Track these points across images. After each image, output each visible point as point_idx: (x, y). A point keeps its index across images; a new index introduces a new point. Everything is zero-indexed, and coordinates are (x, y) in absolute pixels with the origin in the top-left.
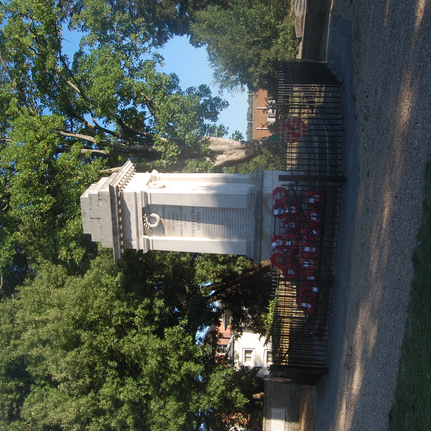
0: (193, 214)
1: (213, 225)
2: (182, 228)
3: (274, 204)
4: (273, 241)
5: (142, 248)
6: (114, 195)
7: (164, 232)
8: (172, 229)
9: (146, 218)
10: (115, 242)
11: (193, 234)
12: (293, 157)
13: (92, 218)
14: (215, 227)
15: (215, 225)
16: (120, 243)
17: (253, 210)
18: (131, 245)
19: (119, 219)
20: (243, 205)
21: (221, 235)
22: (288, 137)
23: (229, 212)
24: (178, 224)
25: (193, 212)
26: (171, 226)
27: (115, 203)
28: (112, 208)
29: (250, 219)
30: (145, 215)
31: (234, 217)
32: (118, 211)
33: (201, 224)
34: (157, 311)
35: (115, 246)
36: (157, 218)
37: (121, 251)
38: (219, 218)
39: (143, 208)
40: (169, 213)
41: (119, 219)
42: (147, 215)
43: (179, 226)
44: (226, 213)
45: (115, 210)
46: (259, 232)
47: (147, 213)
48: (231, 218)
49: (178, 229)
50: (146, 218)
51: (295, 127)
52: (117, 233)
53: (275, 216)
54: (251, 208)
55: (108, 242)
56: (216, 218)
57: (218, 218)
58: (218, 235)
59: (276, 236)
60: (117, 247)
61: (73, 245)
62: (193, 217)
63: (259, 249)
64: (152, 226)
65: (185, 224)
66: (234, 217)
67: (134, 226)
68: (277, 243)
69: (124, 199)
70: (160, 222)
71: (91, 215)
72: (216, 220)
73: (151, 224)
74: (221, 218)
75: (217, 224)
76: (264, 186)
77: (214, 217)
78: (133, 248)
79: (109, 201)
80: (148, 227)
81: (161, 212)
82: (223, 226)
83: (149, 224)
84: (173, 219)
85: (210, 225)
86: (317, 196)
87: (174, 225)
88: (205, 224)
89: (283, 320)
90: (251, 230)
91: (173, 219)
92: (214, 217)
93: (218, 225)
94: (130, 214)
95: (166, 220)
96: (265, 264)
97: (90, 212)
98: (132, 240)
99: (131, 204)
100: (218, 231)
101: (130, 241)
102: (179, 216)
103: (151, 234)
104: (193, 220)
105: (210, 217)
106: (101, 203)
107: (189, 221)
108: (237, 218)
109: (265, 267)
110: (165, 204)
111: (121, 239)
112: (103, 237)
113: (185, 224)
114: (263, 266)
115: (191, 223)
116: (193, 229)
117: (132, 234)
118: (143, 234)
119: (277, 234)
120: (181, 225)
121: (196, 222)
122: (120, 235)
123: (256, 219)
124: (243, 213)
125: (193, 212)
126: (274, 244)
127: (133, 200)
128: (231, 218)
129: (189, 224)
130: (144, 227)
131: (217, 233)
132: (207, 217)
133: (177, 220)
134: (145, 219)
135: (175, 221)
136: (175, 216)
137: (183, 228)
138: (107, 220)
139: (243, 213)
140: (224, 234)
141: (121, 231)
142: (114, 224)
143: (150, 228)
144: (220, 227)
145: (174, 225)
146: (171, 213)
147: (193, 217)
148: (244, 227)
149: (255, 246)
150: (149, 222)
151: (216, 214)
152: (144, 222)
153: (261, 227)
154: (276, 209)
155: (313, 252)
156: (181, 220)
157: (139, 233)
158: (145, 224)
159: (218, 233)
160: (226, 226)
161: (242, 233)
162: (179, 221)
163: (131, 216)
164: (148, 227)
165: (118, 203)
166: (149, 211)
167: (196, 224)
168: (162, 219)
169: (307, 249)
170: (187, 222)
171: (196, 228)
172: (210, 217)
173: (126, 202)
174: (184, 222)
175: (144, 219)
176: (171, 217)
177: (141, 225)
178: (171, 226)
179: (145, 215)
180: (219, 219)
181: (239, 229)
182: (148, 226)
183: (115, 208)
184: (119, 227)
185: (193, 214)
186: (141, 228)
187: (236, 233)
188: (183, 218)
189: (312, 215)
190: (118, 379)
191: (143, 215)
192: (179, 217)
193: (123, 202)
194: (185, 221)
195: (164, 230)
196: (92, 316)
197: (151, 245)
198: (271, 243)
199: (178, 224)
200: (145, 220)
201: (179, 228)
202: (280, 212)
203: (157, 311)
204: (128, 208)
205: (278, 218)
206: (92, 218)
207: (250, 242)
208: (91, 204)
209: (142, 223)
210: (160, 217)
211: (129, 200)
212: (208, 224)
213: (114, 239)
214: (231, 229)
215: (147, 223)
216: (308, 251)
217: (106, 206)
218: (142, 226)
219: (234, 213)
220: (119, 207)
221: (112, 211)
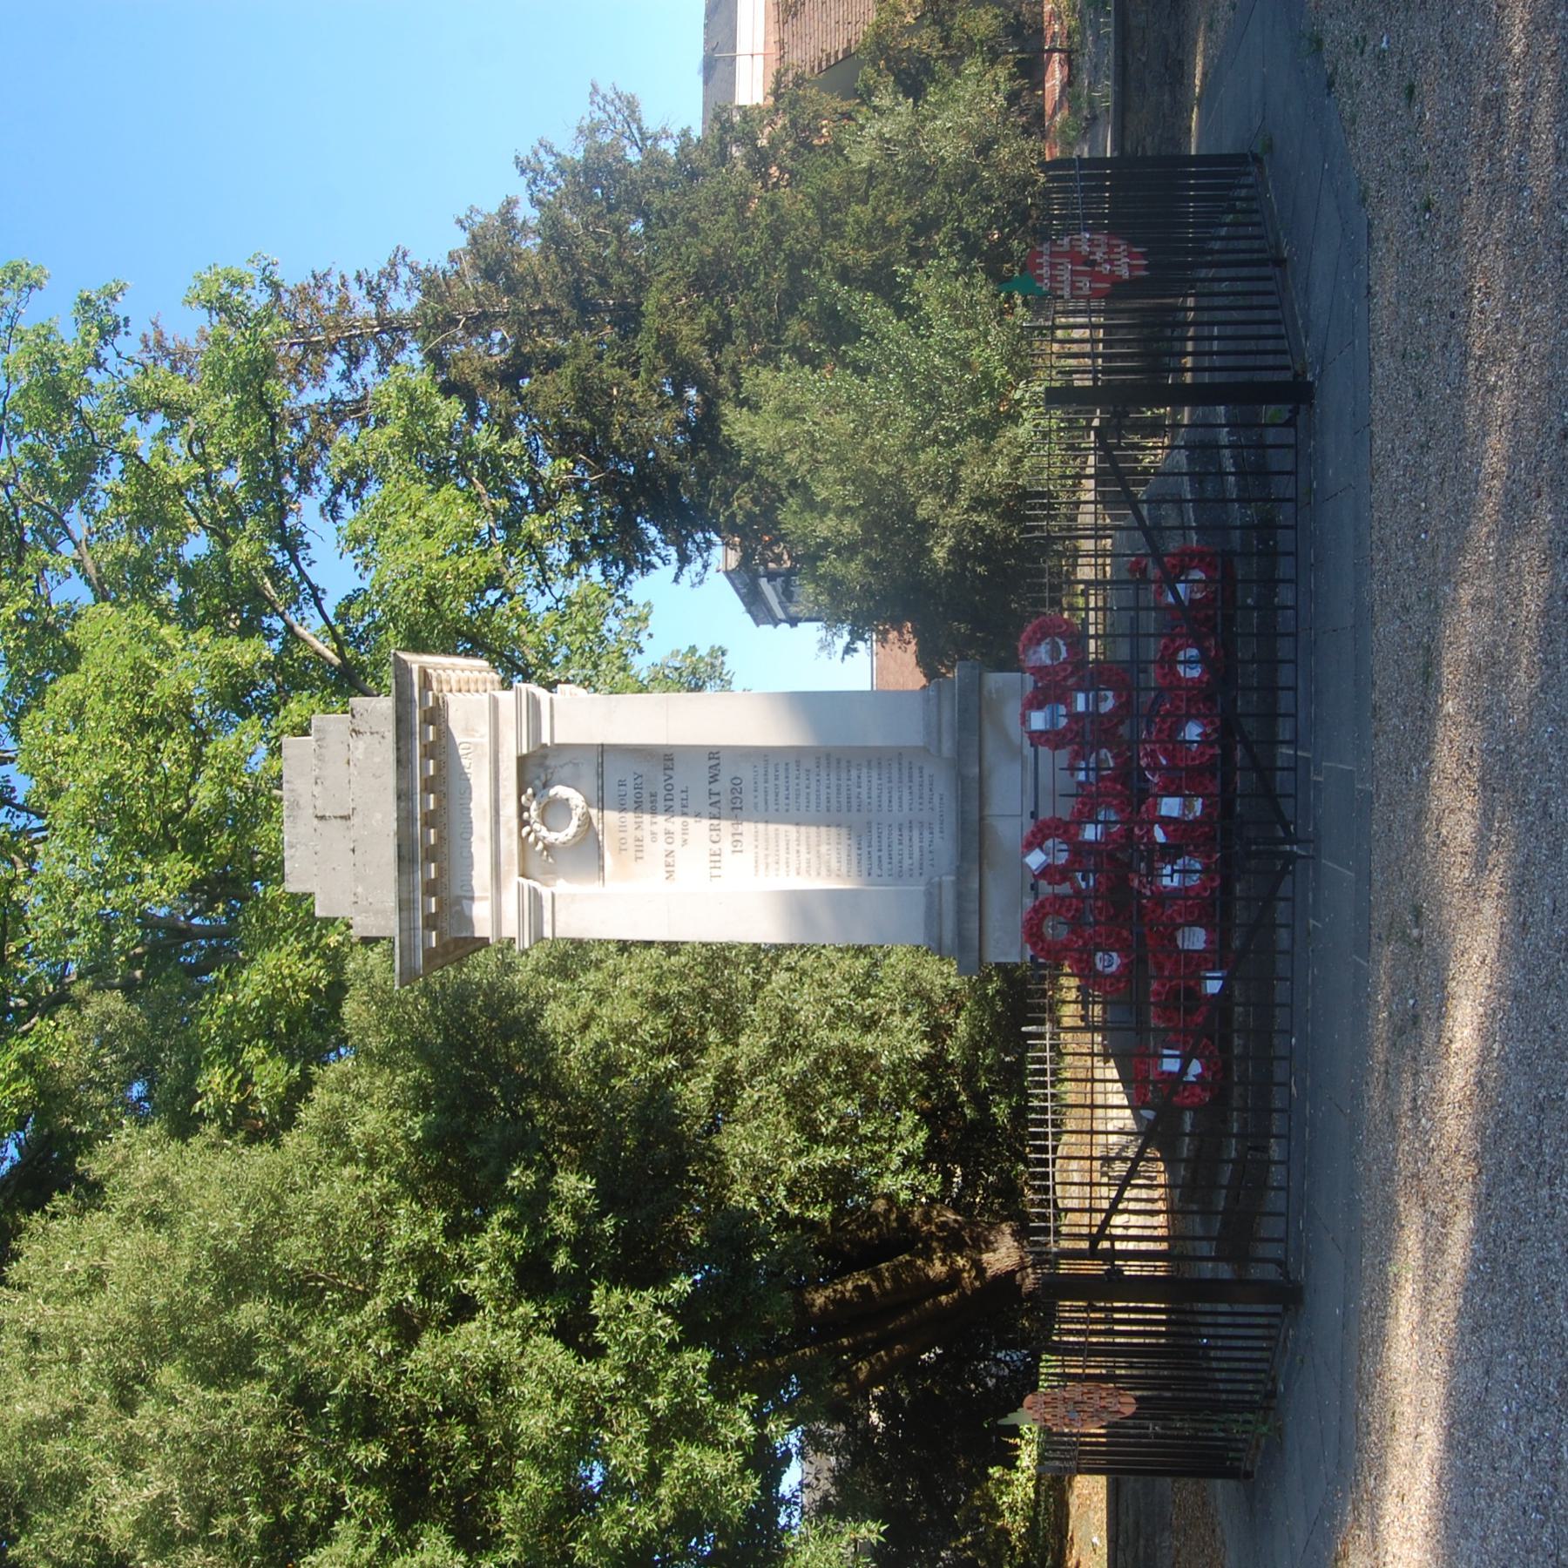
0: (715, 787)
1: (792, 829)
2: (670, 848)
3: (1029, 688)
4: (1029, 846)
5: (510, 929)
6: (412, 700)
7: (602, 868)
8: (631, 852)
9: (534, 806)
10: (405, 896)
11: (716, 872)
12: (1093, 561)
13: (322, 818)
14: (803, 838)
15: (803, 829)
16: (426, 906)
17: (947, 747)
18: (469, 922)
19: (424, 802)
20: (911, 734)
21: (824, 871)
22: (1073, 282)
23: (854, 773)
24: (655, 828)
25: (714, 779)
26: (631, 841)
27: (412, 734)
28: (398, 742)
29: (936, 799)
30: (530, 791)
31: (875, 793)
32: (424, 768)
33: (747, 828)
34: (564, 1223)
35: (405, 914)
36: (573, 803)
37: (426, 939)
38: (818, 797)
39: (522, 761)
40: (622, 784)
41: (424, 802)
42: (534, 795)
43: (661, 837)
44: (844, 775)
45: (410, 761)
46: (973, 839)
47: (537, 782)
48: (864, 796)
49: (656, 850)
50: (534, 806)
51: (1098, 256)
52: (413, 861)
53: (1036, 738)
54: (940, 741)
55: (376, 913)
56: (803, 800)
57: (813, 797)
58: (813, 873)
59: (1044, 822)
60: (413, 920)
61: (251, 1055)
62: (715, 799)
63: (975, 906)
64: (552, 837)
65: (685, 831)
66: (875, 793)
67: (482, 839)
68: (1047, 854)
69: (451, 725)
70: (587, 821)
71: (319, 803)
72: (803, 808)
73: (549, 830)
74: (823, 798)
75: (808, 823)
76: (987, 812)
77: (798, 796)
78: (477, 934)
79: (390, 736)
80: (540, 845)
81: (590, 781)
82: (833, 830)
83: (544, 832)
84: (638, 808)
85: (782, 828)
86: (1198, 575)
87: (639, 833)
88: (761, 826)
89: (1092, 657)
90: (944, 845)
91: (636, 810)
92: (798, 796)
93: (813, 830)
94: (469, 788)
95: (612, 816)
96: (998, 1265)
97: (317, 790)
98: (472, 899)
99: (476, 745)
100: (813, 852)
101: (465, 902)
102: (662, 793)
103: (551, 873)
104: (715, 811)
105: (782, 793)
106: (360, 746)
107: (698, 815)
108: (885, 798)
109: (995, 1277)
110: (606, 742)
111: (431, 888)
112: (360, 890)
113: (685, 831)
114: (989, 1273)
115: (706, 823)
116: (715, 847)
117: (474, 873)
118: (516, 869)
119: (1045, 814)
120: (668, 833)
121: (727, 819)
122: (426, 871)
123: (961, 779)
124: (910, 777)
125: (714, 779)
126: (1036, 859)
127: (484, 729)
128: (864, 796)
129: (700, 828)
130: (523, 841)
131: (809, 861)
132: (771, 797)
133: (654, 812)
134: (528, 810)
135: (647, 818)
136: (646, 798)
137: (677, 846)
138: (379, 816)
139: (910, 777)
140: (834, 864)
141: (431, 854)
142: (405, 820)
143: (546, 847)
144: (819, 836)
145: (639, 833)
146: (630, 783)
147: (715, 799)
148: (916, 834)
149: (960, 896)
150: (544, 823)
151: (803, 783)
152: (523, 823)
153: (981, 819)
154: (1040, 707)
155: (1196, 820)
156: (668, 810)
157: (504, 868)
158: (527, 829)
159: (814, 860)
160: (844, 831)
161: (906, 856)
162: (660, 819)
163: (476, 866)
164: (540, 845)
165: (424, 734)
166: (543, 778)
167: (726, 825)
168: (594, 812)
169: (1170, 806)
170: (691, 820)
171: (726, 845)
172: (782, 793)
173: (458, 740)
174: (678, 821)
175: (522, 809)
176: (630, 801)
177: (510, 835)
178: (631, 841)
179: (530, 791)
180: (818, 805)
181: (896, 841)
182: (537, 840)
183: (411, 751)
184: (425, 836)
185: (715, 787)
186: (510, 844)
187: (885, 860)
188: (677, 804)
189: (1181, 657)
190: (387, 1530)
191: (521, 791)
192: (660, 798)
193: (444, 734)
194: (684, 814)
195: (601, 857)
196: (296, 1251)
197: (547, 916)
198: (1024, 856)
199: (655, 828)
200: (526, 815)
201: (661, 846)
202: (1053, 720)
203: (564, 1223)
204: (465, 762)
205: (1047, 743)
206: (322, 818)
207: (940, 885)
208: (320, 758)
209: (514, 823)
210: (589, 805)
211: (468, 730)
212: (772, 827)
213: (399, 779)
214: (864, 844)
215: (537, 826)
216: (1175, 814)
217: (377, 760)
218: (515, 836)
219: (874, 774)
220: (430, 751)
221: (399, 761)
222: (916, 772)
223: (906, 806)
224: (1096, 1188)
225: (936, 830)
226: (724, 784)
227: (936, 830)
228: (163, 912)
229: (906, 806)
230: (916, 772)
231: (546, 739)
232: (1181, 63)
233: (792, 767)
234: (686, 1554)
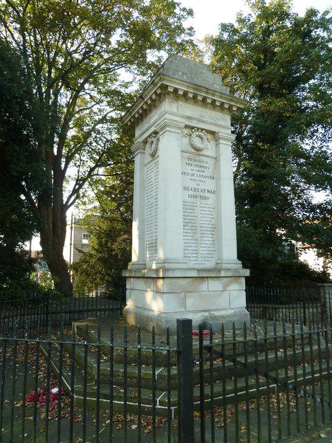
0: (206, 191)
25: (208, 191)
43: (193, 172)
48: (205, 239)
125: (208, 191)
146: (207, 165)
152: (198, 129)
222: (211, 256)
223: (202, 252)
224: (222, 431)
225: (196, 262)
226: (207, 194)
227: (196, 262)
228: (59, 100)
229: (202, 252)
230: (211, 256)
231: (221, 141)
232: (250, 296)
233: (212, 216)
234: (145, 11)
